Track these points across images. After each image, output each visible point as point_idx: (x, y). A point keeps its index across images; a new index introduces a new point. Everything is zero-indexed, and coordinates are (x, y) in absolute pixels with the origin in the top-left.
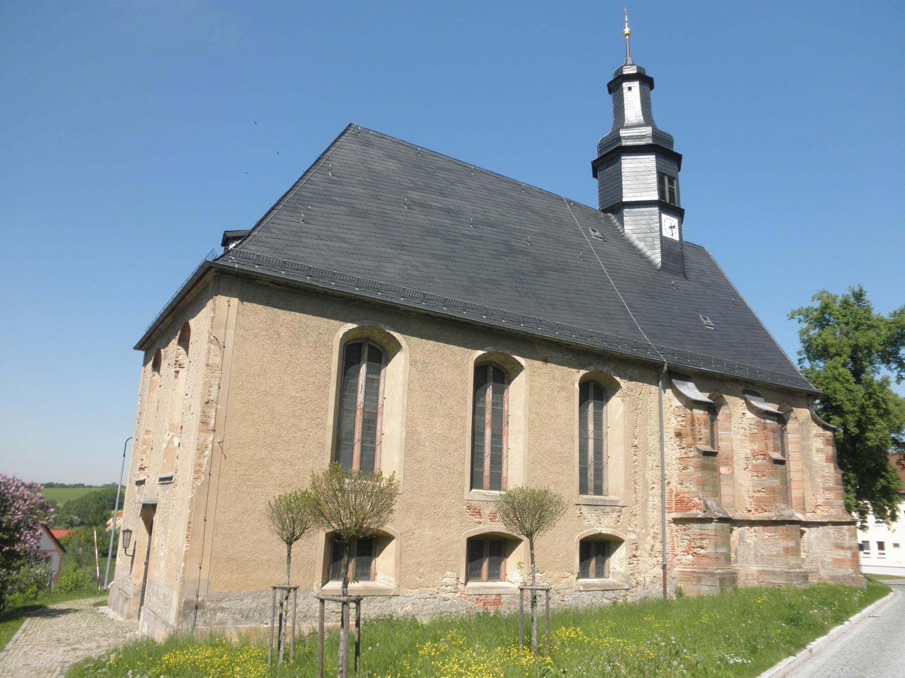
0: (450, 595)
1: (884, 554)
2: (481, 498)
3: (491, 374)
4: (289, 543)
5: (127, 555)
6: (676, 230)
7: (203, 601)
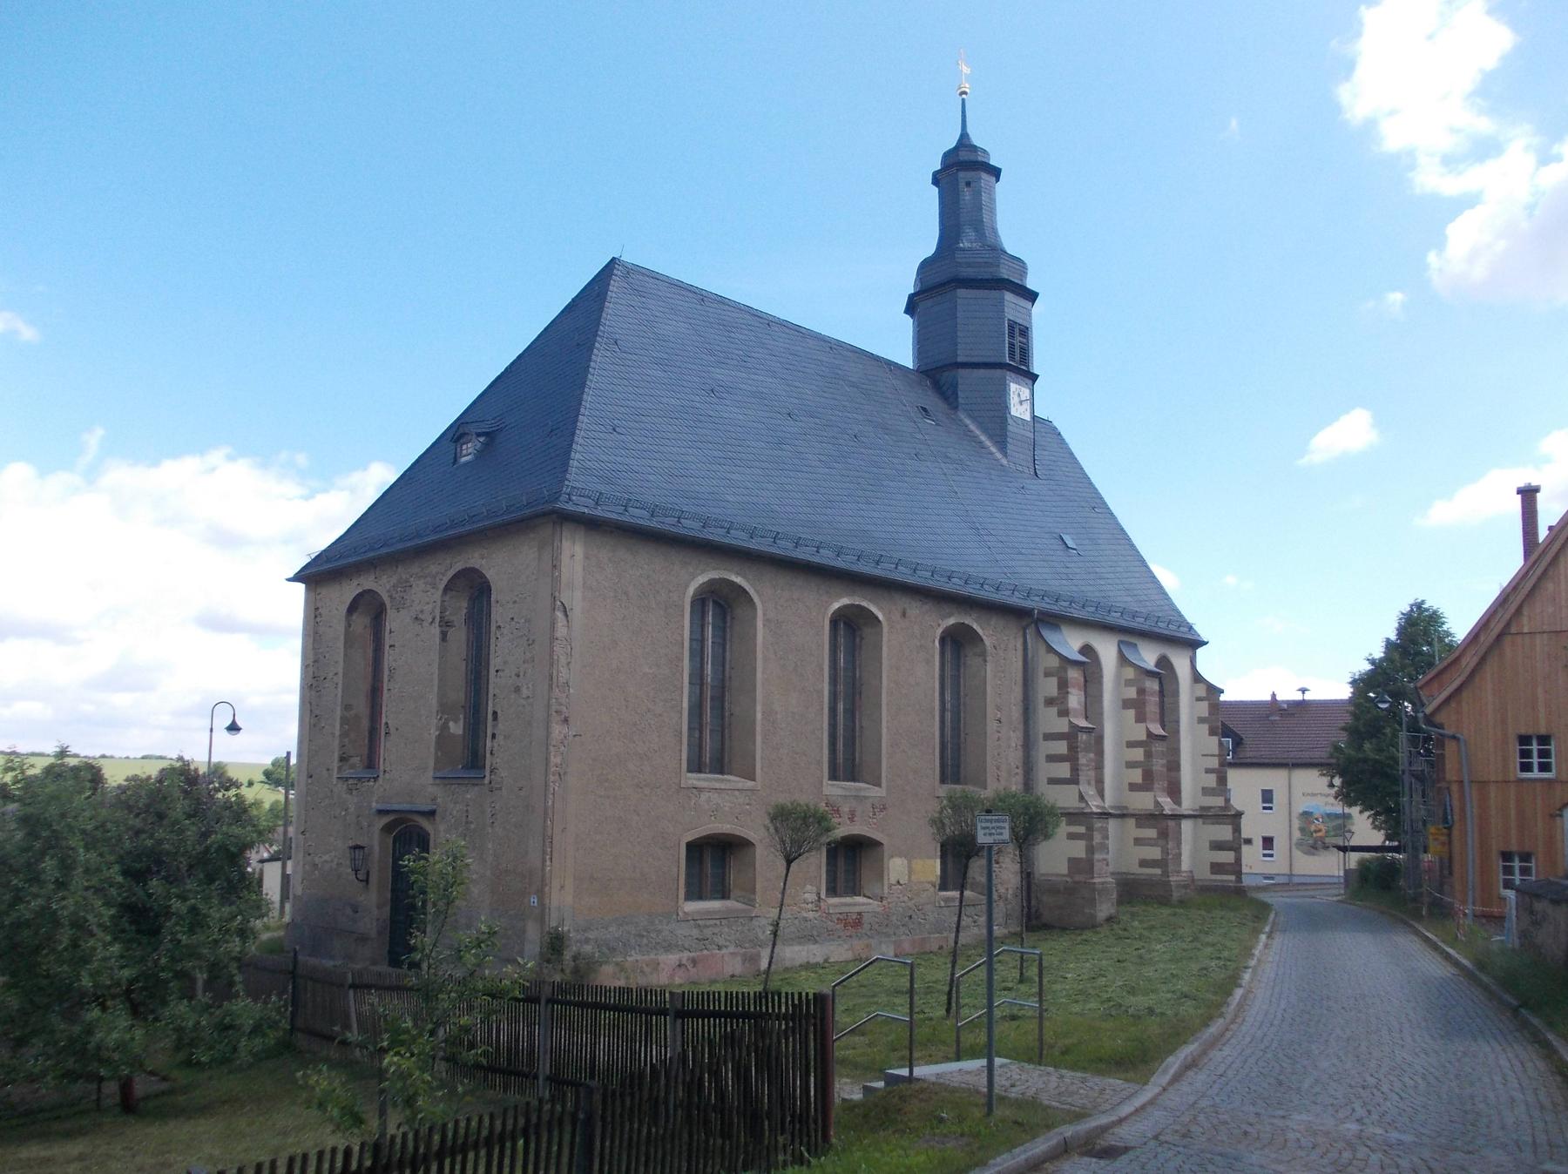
0: (811, 915)
1: (1271, 856)
2: (840, 792)
3: (842, 633)
4: (789, 862)
5: (357, 879)
6: (1027, 406)
7: (569, 931)
